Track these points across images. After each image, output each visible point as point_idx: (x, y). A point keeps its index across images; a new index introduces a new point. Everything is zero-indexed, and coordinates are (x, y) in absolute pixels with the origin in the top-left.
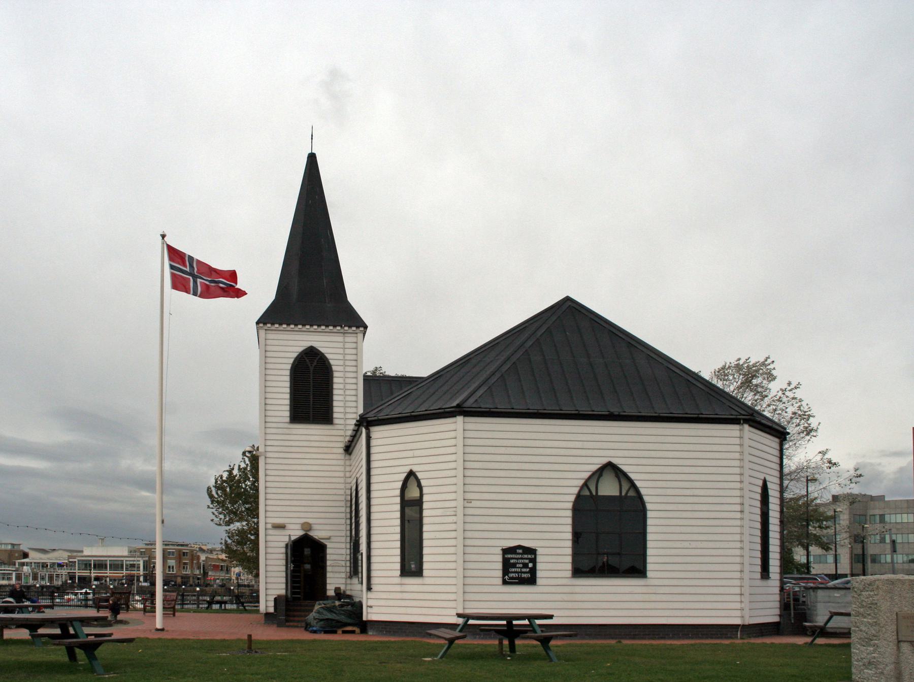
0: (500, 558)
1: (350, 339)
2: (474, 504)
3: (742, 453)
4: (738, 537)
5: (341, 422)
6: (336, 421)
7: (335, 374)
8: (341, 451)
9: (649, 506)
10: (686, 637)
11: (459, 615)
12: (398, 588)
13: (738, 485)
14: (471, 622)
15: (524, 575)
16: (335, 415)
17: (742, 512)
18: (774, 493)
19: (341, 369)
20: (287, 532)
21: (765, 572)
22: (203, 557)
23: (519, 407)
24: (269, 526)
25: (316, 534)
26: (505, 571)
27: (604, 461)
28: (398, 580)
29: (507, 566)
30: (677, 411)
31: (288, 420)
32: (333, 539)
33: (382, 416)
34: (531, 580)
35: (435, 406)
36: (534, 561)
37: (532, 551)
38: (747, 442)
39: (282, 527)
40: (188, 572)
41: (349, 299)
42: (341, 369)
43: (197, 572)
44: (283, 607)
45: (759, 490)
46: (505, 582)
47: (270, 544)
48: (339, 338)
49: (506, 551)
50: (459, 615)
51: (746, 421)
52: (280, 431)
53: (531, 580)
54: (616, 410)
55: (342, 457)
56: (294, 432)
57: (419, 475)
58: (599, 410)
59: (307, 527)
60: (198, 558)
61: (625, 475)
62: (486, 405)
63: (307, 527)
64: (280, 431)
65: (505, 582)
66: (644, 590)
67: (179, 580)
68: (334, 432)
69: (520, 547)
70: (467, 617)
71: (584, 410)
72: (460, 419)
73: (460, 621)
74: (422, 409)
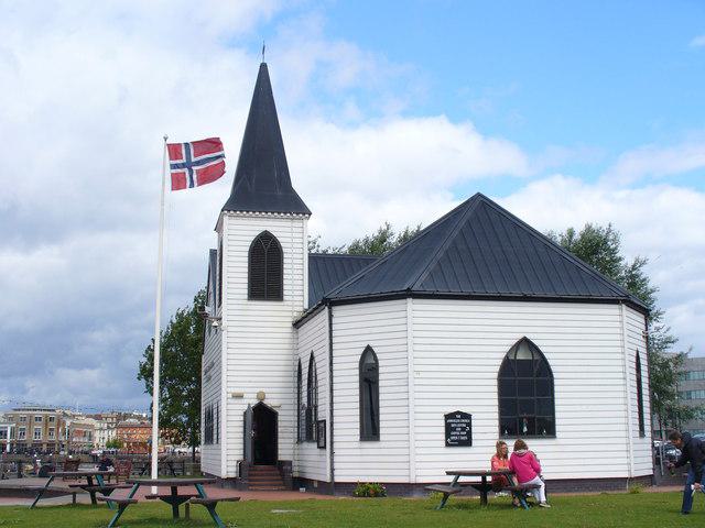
0: (443, 423)
1: (297, 224)
2: (616, 349)
3: (622, 328)
4: (622, 401)
5: (290, 298)
6: (285, 298)
7: (285, 255)
8: (291, 325)
9: (555, 375)
10: (588, 489)
11: (449, 473)
12: (358, 452)
13: (621, 356)
14: (462, 479)
15: (462, 438)
16: (285, 293)
17: (624, 379)
18: (644, 362)
19: (289, 245)
20: (245, 401)
21: (209, 416)
22: (68, 423)
23: (455, 291)
24: (230, 395)
25: (269, 402)
26: (448, 435)
27: (520, 336)
28: (358, 445)
29: (449, 430)
30: (573, 294)
31: (246, 297)
32: (283, 407)
33: (343, 296)
34: (468, 443)
35: (387, 290)
36: (469, 425)
37: (467, 416)
38: (626, 319)
39: (240, 396)
40: (54, 438)
41: (294, 186)
42: (289, 245)
43: (63, 439)
44: (245, 473)
45: (634, 360)
46: (448, 445)
47: (623, 427)
48: (289, 223)
49: (448, 417)
50: (449, 473)
51: (624, 302)
52: (240, 307)
53: (468, 443)
54: (528, 293)
55: (290, 330)
56: (251, 307)
57: (375, 350)
58: (516, 293)
59: (261, 396)
60: (64, 423)
61: (536, 348)
62: (430, 289)
63: (261, 396)
64: (240, 307)
65: (448, 445)
66: (556, 448)
67: (45, 448)
68: (285, 308)
69: (458, 413)
70: (458, 474)
71: (504, 292)
72: (410, 300)
73: (451, 479)
74: (376, 292)
